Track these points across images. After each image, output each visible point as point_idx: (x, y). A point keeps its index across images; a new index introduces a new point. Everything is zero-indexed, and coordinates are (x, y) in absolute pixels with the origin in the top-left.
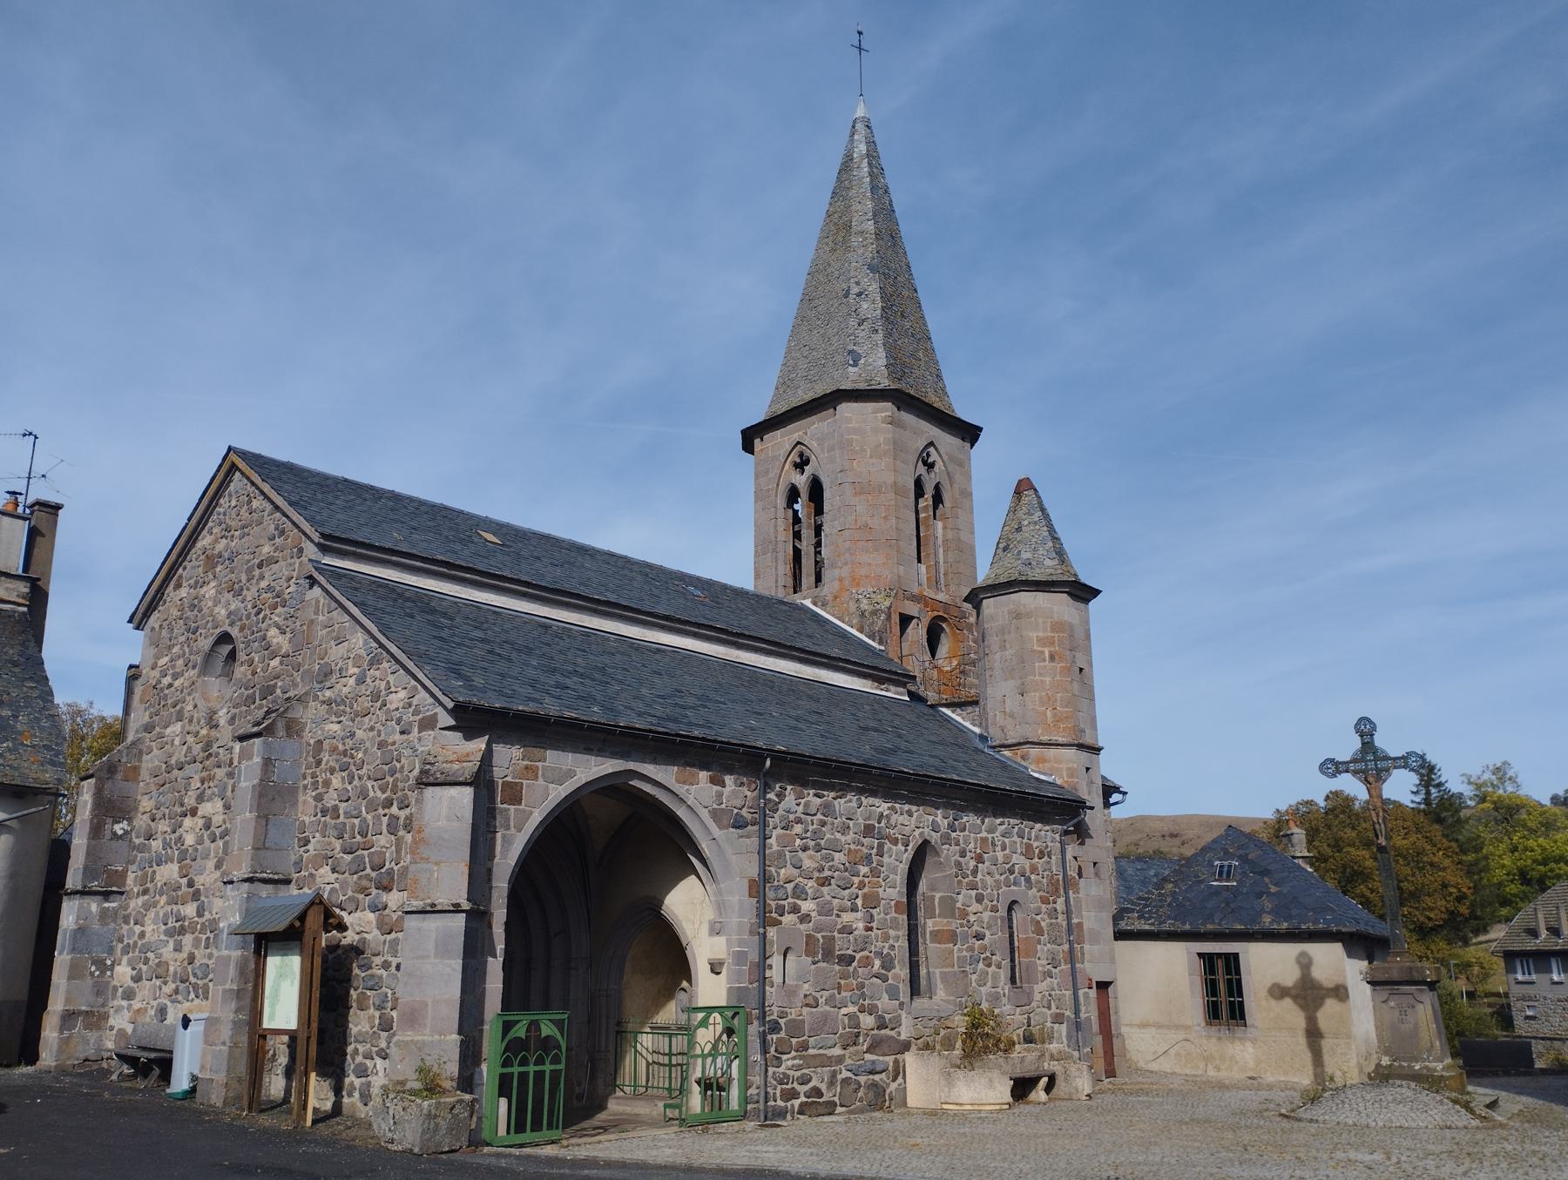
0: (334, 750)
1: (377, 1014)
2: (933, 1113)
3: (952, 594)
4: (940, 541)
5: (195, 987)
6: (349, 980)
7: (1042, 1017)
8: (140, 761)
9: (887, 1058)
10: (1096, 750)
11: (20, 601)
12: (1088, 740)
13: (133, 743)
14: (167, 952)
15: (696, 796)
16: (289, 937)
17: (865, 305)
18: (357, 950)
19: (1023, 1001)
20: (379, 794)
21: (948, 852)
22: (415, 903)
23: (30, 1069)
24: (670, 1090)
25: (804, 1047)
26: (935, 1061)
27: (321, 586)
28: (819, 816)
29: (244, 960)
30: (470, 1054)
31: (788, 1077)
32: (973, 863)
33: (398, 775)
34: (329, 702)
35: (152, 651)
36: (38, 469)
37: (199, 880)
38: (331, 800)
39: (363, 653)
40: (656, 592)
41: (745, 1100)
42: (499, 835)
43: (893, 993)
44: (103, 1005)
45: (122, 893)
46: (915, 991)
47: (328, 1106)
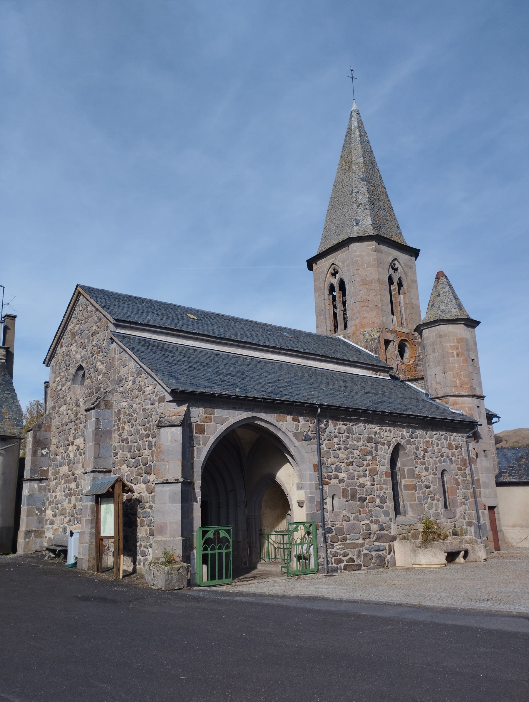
0: (125, 413)
1: (148, 528)
2: (408, 569)
3: (408, 329)
4: (402, 305)
5: (77, 518)
6: (136, 514)
7: (461, 523)
8: (51, 422)
9: (385, 544)
10: (482, 397)
11: (2, 357)
12: (478, 393)
13: (48, 415)
14: (66, 504)
15: (286, 428)
16: (107, 496)
17: (360, 197)
18: (139, 501)
19: (452, 516)
20: (144, 432)
21: (410, 448)
22: (159, 479)
23: (14, 555)
24: (284, 560)
25: (345, 539)
26: (408, 545)
27: (116, 342)
28: (346, 434)
29: (92, 505)
30: (188, 545)
31: (337, 553)
32: (422, 453)
33: (151, 423)
34: (122, 393)
35: (53, 375)
36: (6, 302)
37: (76, 472)
38: (125, 435)
39: (134, 370)
40: (268, 336)
41: (318, 564)
42: (195, 448)
43: (387, 514)
44: (42, 527)
45: (47, 479)
46: (397, 512)
47: (131, 569)
